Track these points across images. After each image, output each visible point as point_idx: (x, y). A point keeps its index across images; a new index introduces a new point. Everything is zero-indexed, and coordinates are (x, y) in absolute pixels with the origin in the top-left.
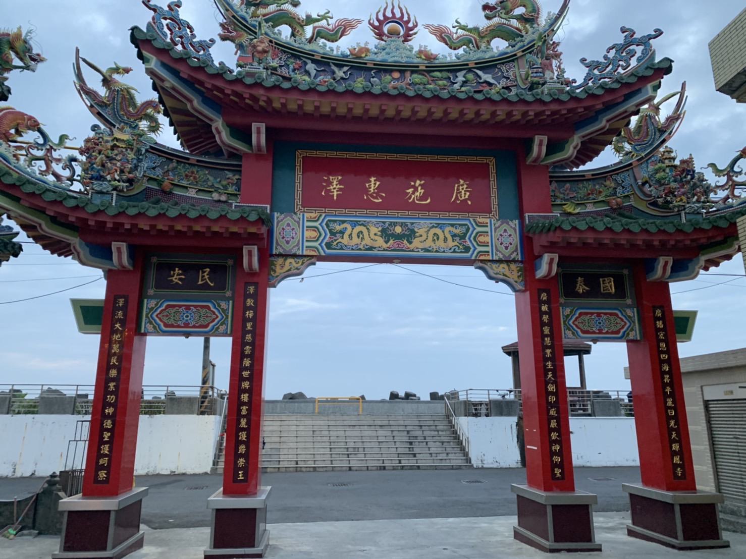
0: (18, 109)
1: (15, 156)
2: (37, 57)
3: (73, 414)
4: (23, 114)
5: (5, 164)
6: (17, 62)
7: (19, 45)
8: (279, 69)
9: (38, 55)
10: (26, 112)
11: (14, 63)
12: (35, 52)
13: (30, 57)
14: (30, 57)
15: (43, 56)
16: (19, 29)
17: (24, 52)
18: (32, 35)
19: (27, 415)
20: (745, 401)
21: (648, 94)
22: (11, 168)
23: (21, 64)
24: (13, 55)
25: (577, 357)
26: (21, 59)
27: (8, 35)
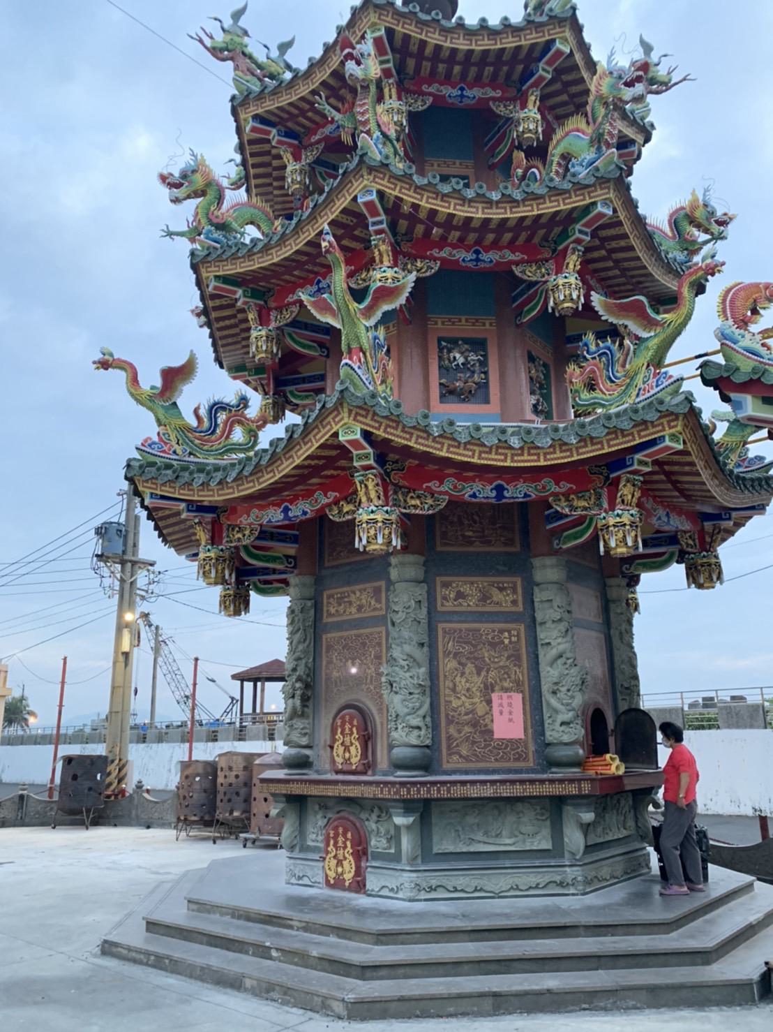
0: (747, 281)
1: (763, 345)
2: (725, 218)
3: (766, 728)
4: (757, 285)
5: (757, 361)
6: (703, 237)
7: (700, 214)
8: (614, 419)
9: (725, 214)
10: (758, 281)
11: (700, 240)
12: (719, 213)
13: (717, 222)
14: (717, 222)
15: (730, 214)
16: (693, 193)
17: (708, 219)
18: (711, 192)
19: (698, 731)
20: (259, 684)
21: (746, 411)
22: (765, 364)
23: (708, 237)
24: (695, 232)
25: (252, 684)
26: (706, 231)
27: (682, 208)
